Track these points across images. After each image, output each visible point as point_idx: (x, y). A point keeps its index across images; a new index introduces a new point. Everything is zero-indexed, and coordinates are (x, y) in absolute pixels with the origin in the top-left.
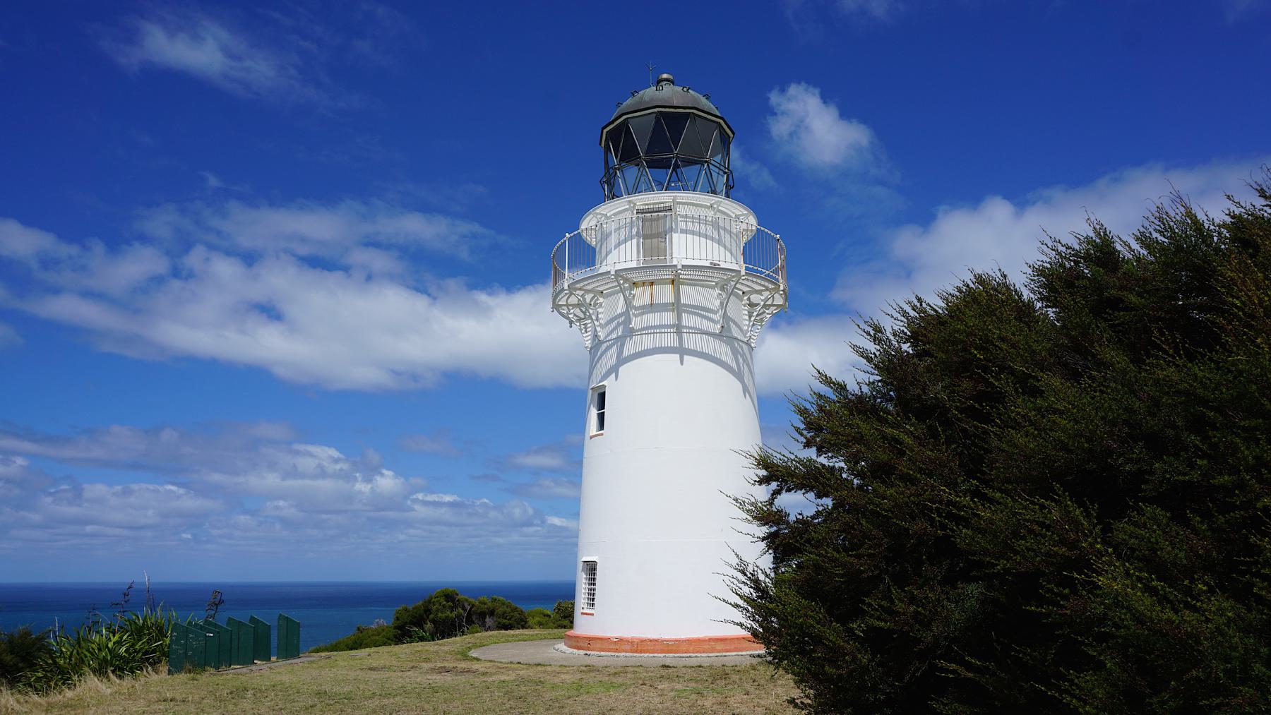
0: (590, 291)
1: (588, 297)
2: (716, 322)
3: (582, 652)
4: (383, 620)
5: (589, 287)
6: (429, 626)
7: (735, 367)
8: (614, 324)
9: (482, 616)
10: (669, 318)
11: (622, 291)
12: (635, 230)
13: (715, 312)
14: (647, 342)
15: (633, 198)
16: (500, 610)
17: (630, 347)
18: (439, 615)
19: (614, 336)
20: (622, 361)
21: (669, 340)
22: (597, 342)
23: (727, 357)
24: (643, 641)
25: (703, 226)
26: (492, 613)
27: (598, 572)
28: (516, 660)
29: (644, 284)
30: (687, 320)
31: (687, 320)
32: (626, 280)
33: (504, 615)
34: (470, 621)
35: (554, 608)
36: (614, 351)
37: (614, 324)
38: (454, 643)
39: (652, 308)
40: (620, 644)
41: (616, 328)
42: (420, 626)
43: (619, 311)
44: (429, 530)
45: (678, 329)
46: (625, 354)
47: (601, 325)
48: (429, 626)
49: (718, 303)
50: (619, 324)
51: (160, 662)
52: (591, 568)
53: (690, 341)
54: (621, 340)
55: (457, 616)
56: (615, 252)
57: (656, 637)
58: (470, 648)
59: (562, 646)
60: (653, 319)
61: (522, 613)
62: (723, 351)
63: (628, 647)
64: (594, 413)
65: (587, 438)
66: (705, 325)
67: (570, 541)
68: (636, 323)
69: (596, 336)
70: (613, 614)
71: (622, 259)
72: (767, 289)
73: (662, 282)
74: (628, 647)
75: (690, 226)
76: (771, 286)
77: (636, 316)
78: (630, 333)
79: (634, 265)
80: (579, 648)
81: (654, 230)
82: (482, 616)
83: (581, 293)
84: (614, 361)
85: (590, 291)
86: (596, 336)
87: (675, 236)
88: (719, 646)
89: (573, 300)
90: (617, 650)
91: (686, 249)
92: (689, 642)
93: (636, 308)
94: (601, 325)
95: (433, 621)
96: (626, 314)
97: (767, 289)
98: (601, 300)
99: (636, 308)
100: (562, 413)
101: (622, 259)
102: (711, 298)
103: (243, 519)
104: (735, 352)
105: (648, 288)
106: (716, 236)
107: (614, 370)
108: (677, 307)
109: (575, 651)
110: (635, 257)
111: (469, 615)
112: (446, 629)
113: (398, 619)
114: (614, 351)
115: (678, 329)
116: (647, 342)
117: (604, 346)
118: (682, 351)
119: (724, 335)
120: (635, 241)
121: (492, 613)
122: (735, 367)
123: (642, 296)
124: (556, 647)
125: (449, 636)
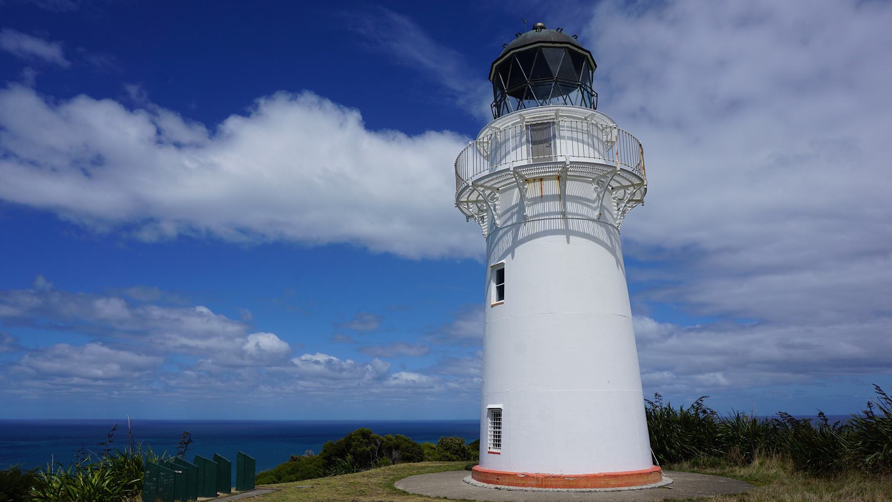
0: (488, 188)
1: (488, 192)
2: (595, 209)
3: (492, 486)
4: (311, 453)
5: (488, 185)
6: (349, 457)
7: (609, 244)
8: (509, 214)
9: (390, 450)
10: (555, 206)
11: (518, 186)
12: (524, 139)
13: (594, 202)
14: (539, 226)
15: (523, 112)
16: (404, 445)
17: (524, 231)
18: (356, 449)
19: (509, 223)
20: (516, 243)
21: (558, 224)
22: (494, 230)
23: (604, 237)
24: (547, 477)
25: (580, 135)
26: (397, 447)
27: (503, 417)
28: (438, 493)
29: (534, 180)
30: (571, 207)
31: (571, 207)
32: (521, 176)
33: (407, 449)
34: (381, 455)
35: (459, 446)
36: (509, 237)
37: (509, 214)
38: (377, 474)
39: (542, 198)
40: (526, 480)
41: (511, 217)
42: (343, 457)
43: (514, 203)
44: (394, 387)
45: (564, 215)
46: (520, 237)
47: (497, 214)
48: (349, 457)
49: (595, 195)
50: (513, 215)
51: (137, 494)
52: (496, 415)
53: (574, 225)
54: (516, 226)
55: (372, 450)
56: (513, 154)
57: (557, 473)
58: (394, 480)
59: (469, 478)
60: (539, 208)
61: (419, 447)
62: (600, 232)
63: (534, 483)
64: (494, 287)
65: (488, 307)
66: (584, 210)
67: (478, 393)
68: (529, 212)
69: (493, 224)
70: (520, 451)
71: (519, 158)
72: (633, 185)
73: (549, 178)
74: (534, 483)
75: (575, 135)
76: (637, 181)
77: (529, 206)
78: (524, 219)
79: (525, 163)
80: (488, 482)
81: (541, 136)
82: (390, 450)
83: (482, 189)
84: (510, 244)
85: (488, 188)
86: (493, 224)
87: (558, 141)
88: (613, 482)
89: (473, 197)
90: (523, 485)
91: (567, 150)
92: (587, 478)
93: (528, 200)
94: (497, 214)
95: (353, 454)
96: (521, 206)
97: (633, 185)
98: (498, 195)
99: (528, 200)
100: (455, 286)
101: (519, 158)
102: (589, 191)
103: (189, 373)
104: (609, 233)
105: (538, 184)
106: (590, 142)
107: (511, 251)
108: (562, 197)
109: (486, 485)
110: (525, 156)
111: (380, 449)
112: (363, 462)
113: (325, 451)
114: (509, 237)
115: (564, 215)
116: (539, 226)
117: (501, 233)
118: (568, 233)
119: (600, 220)
120: (524, 147)
121: (397, 447)
122: (609, 244)
123: (533, 190)
124: (465, 479)
125: (368, 467)
